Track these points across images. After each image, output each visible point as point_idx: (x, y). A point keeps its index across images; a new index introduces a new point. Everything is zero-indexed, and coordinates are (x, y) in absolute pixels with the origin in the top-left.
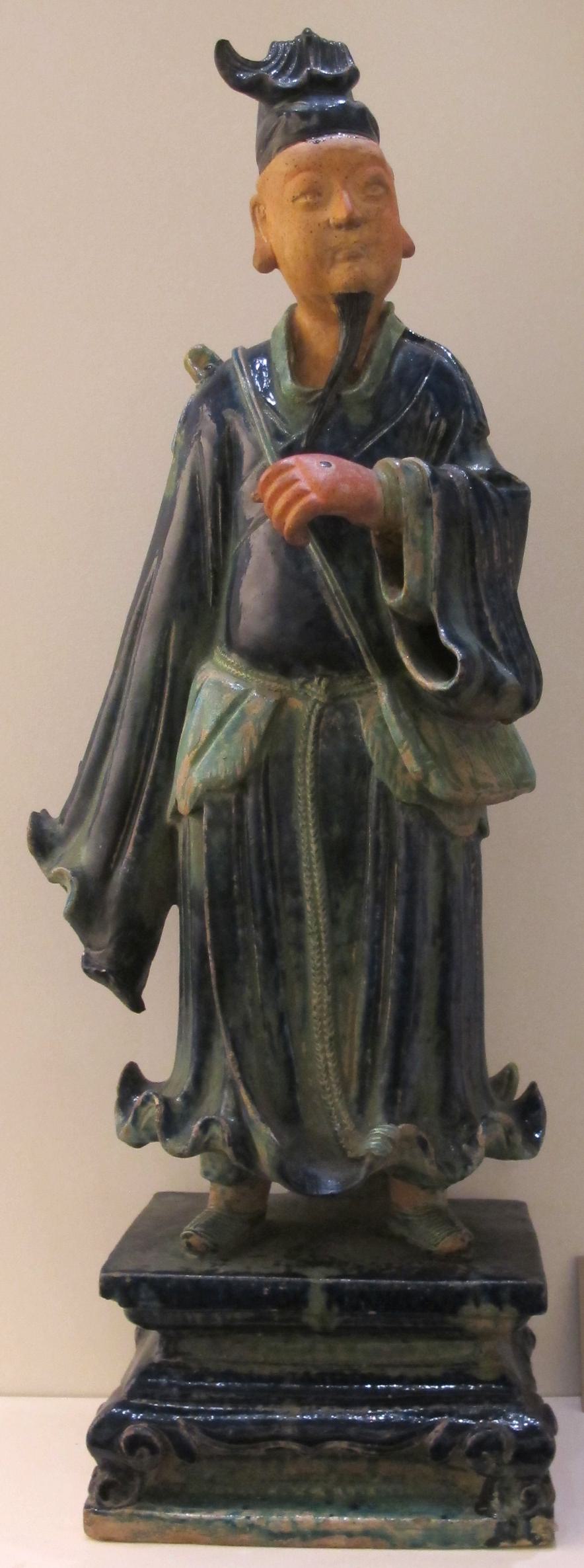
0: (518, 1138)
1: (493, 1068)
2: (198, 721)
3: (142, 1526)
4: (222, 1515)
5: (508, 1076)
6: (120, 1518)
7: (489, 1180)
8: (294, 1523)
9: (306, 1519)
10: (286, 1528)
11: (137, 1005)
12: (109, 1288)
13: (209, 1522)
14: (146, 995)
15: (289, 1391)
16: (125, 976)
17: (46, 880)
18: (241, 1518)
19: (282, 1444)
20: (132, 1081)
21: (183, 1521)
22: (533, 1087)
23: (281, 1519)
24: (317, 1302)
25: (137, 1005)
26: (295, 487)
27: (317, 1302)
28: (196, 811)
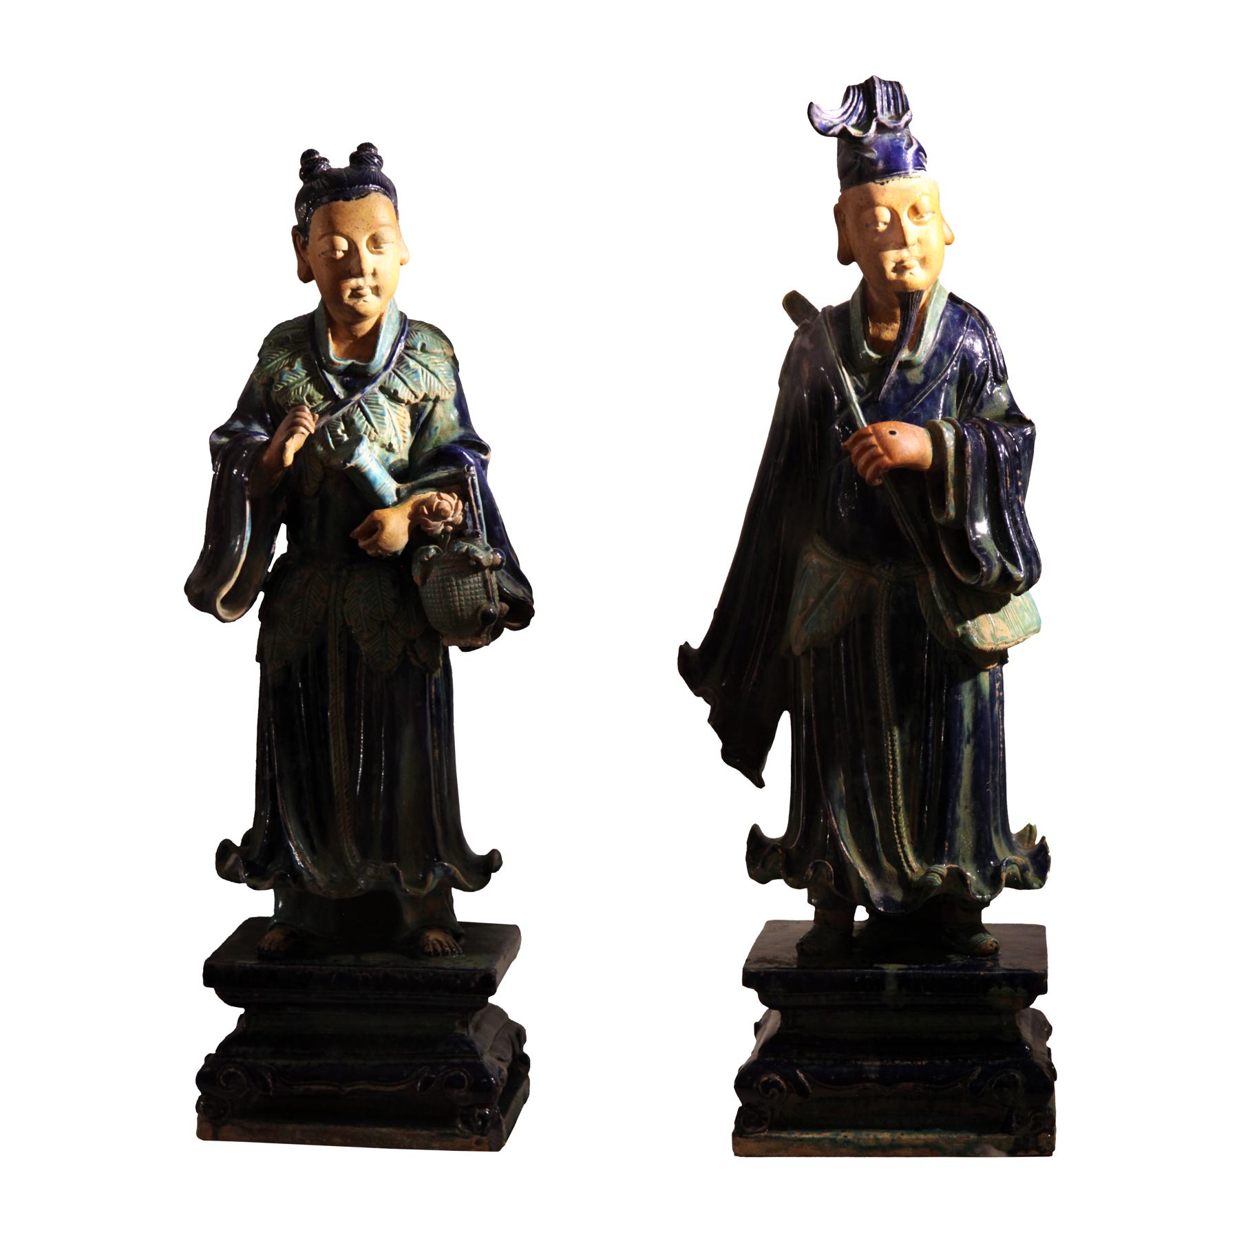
0: (1030, 875)
1: (1015, 827)
2: (804, 594)
3: (773, 1145)
4: (828, 1135)
5: (1030, 831)
6: (758, 1140)
7: (1005, 909)
8: (877, 1139)
9: (885, 1136)
10: (872, 1144)
11: (760, 784)
12: (750, 979)
13: (819, 1140)
14: (765, 775)
15: (979, 438)
16: (745, 754)
17: (493, 459)
18: (842, 1135)
19: (868, 1085)
20: (755, 836)
21: (802, 1140)
22: (1043, 838)
23: (869, 1136)
24: (891, 987)
25: (760, 784)
26: (865, 441)
27: (891, 987)
28: (806, 653)
